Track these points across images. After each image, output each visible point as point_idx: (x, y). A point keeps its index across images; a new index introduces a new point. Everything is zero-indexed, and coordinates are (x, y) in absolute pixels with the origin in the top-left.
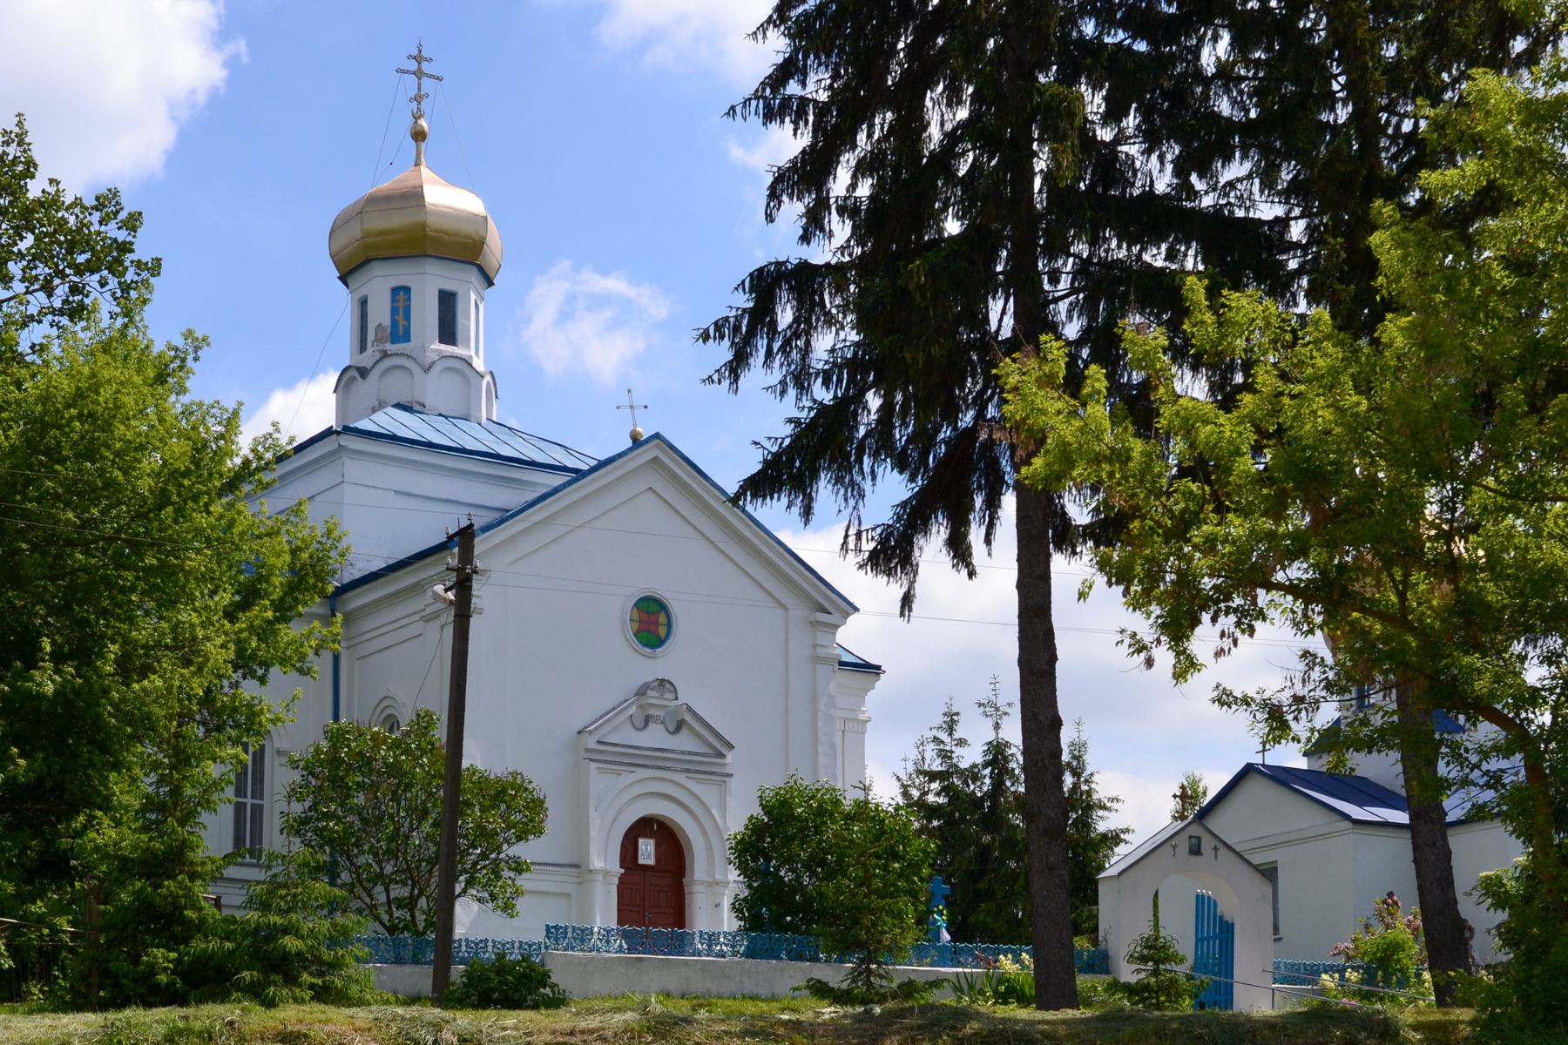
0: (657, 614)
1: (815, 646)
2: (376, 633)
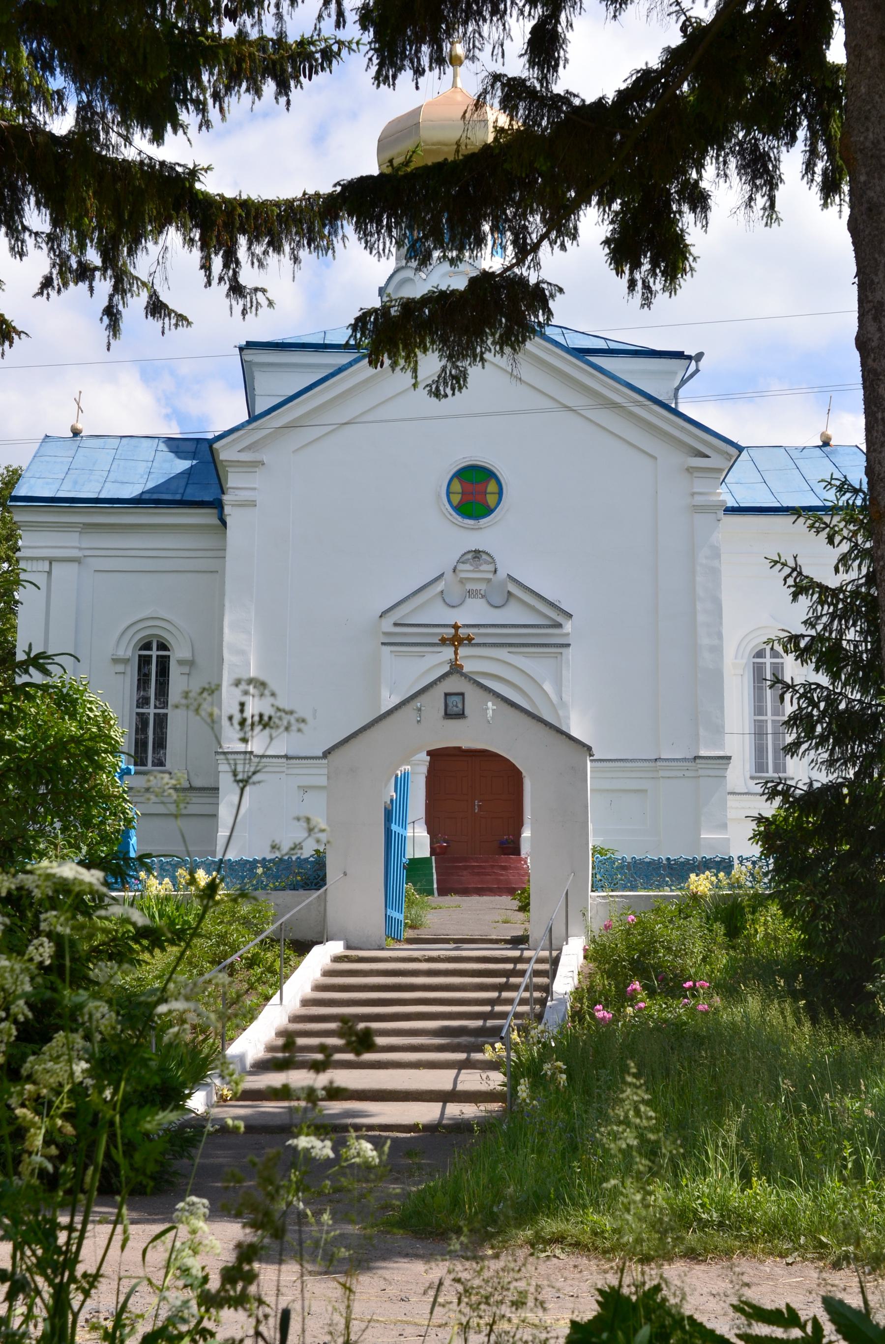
0: (487, 482)
1: (693, 494)
2: (187, 554)
